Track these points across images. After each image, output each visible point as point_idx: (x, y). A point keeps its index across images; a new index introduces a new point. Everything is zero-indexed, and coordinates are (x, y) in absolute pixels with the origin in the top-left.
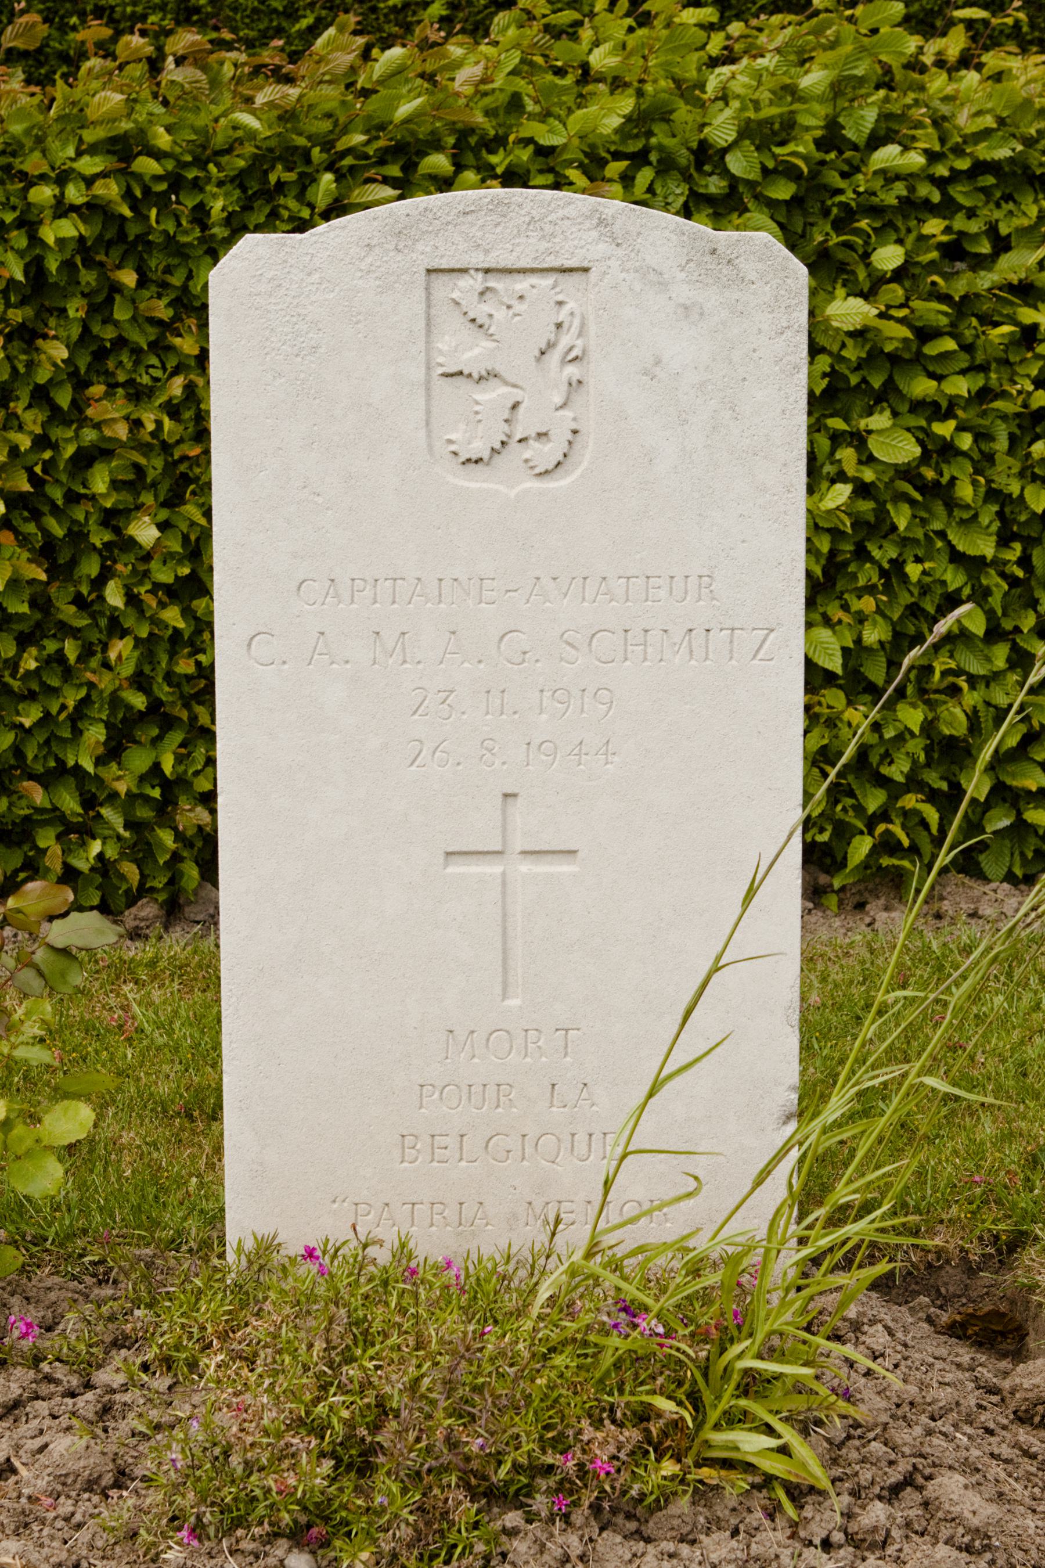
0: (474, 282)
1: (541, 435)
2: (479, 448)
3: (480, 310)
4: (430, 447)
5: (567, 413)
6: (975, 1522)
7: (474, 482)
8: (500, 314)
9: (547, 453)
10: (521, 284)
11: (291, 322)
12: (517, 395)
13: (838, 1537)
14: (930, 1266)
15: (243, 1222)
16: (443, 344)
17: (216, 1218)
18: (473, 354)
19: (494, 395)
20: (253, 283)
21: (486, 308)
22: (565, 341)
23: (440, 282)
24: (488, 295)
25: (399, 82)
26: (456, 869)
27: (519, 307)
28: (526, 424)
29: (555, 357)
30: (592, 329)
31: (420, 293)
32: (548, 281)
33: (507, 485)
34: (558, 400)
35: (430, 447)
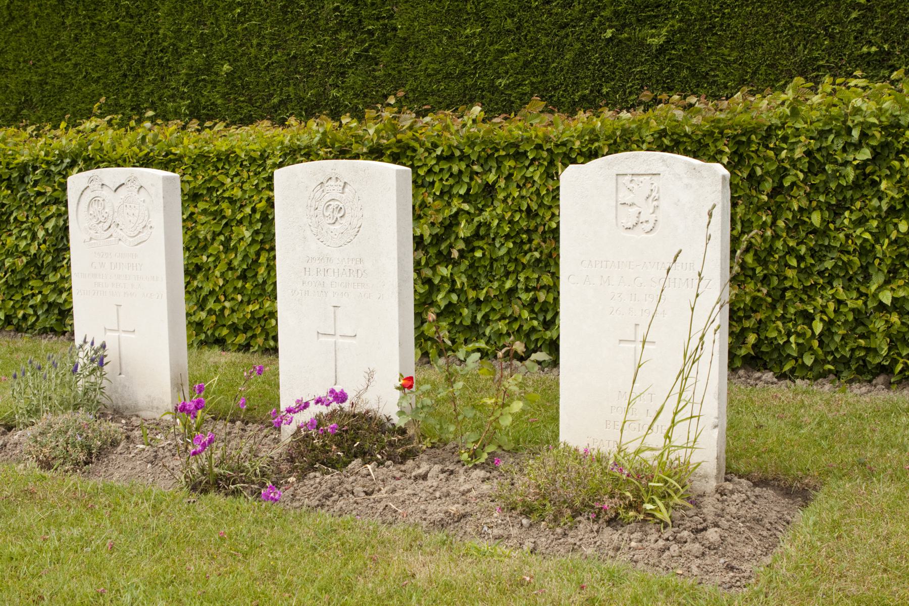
0: (629, 178)
1: (647, 221)
2: (630, 225)
3: (630, 186)
4: (617, 225)
5: (654, 215)
6: (712, 540)
7: (628, 234)
8: (636, 187)
9: (648, 227)
10: (642, 178)
11: (584, 190)
12: (640, 210)
13: (671, 538)
14: (803, 489)
15: (564, 436)
16: (620, 195)
17: (557, 435)
18: (628, 200)
19: (634, 210)
20: (572, 178)
21: (632, 185)
22: (654, 194)
23: (620, 178)
24: (142, 190)
25: (608, 120)
26: (622, 345)
27: (641, 185)
28: (643, 218)
29: (651, 199)
30: (661, 191)
31: (614, 181)
32: (649, 177)
33: (638, 235)
34: (651, 211)
35: (617, 225)
